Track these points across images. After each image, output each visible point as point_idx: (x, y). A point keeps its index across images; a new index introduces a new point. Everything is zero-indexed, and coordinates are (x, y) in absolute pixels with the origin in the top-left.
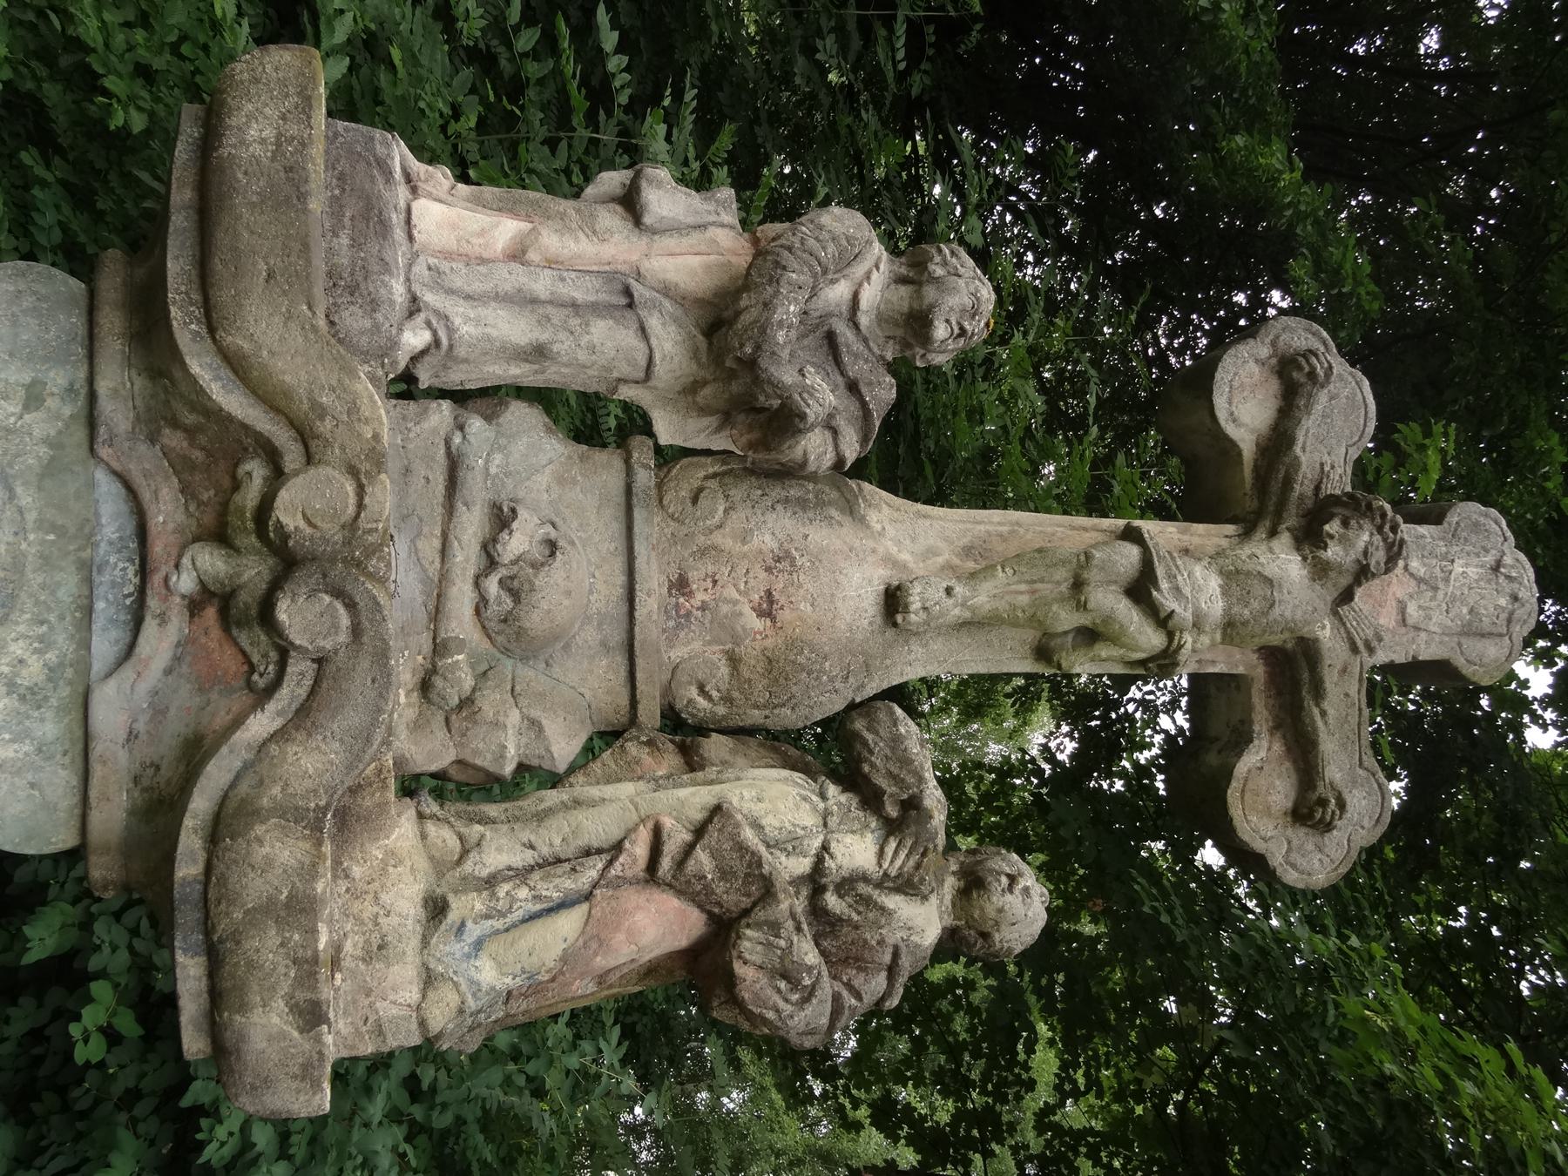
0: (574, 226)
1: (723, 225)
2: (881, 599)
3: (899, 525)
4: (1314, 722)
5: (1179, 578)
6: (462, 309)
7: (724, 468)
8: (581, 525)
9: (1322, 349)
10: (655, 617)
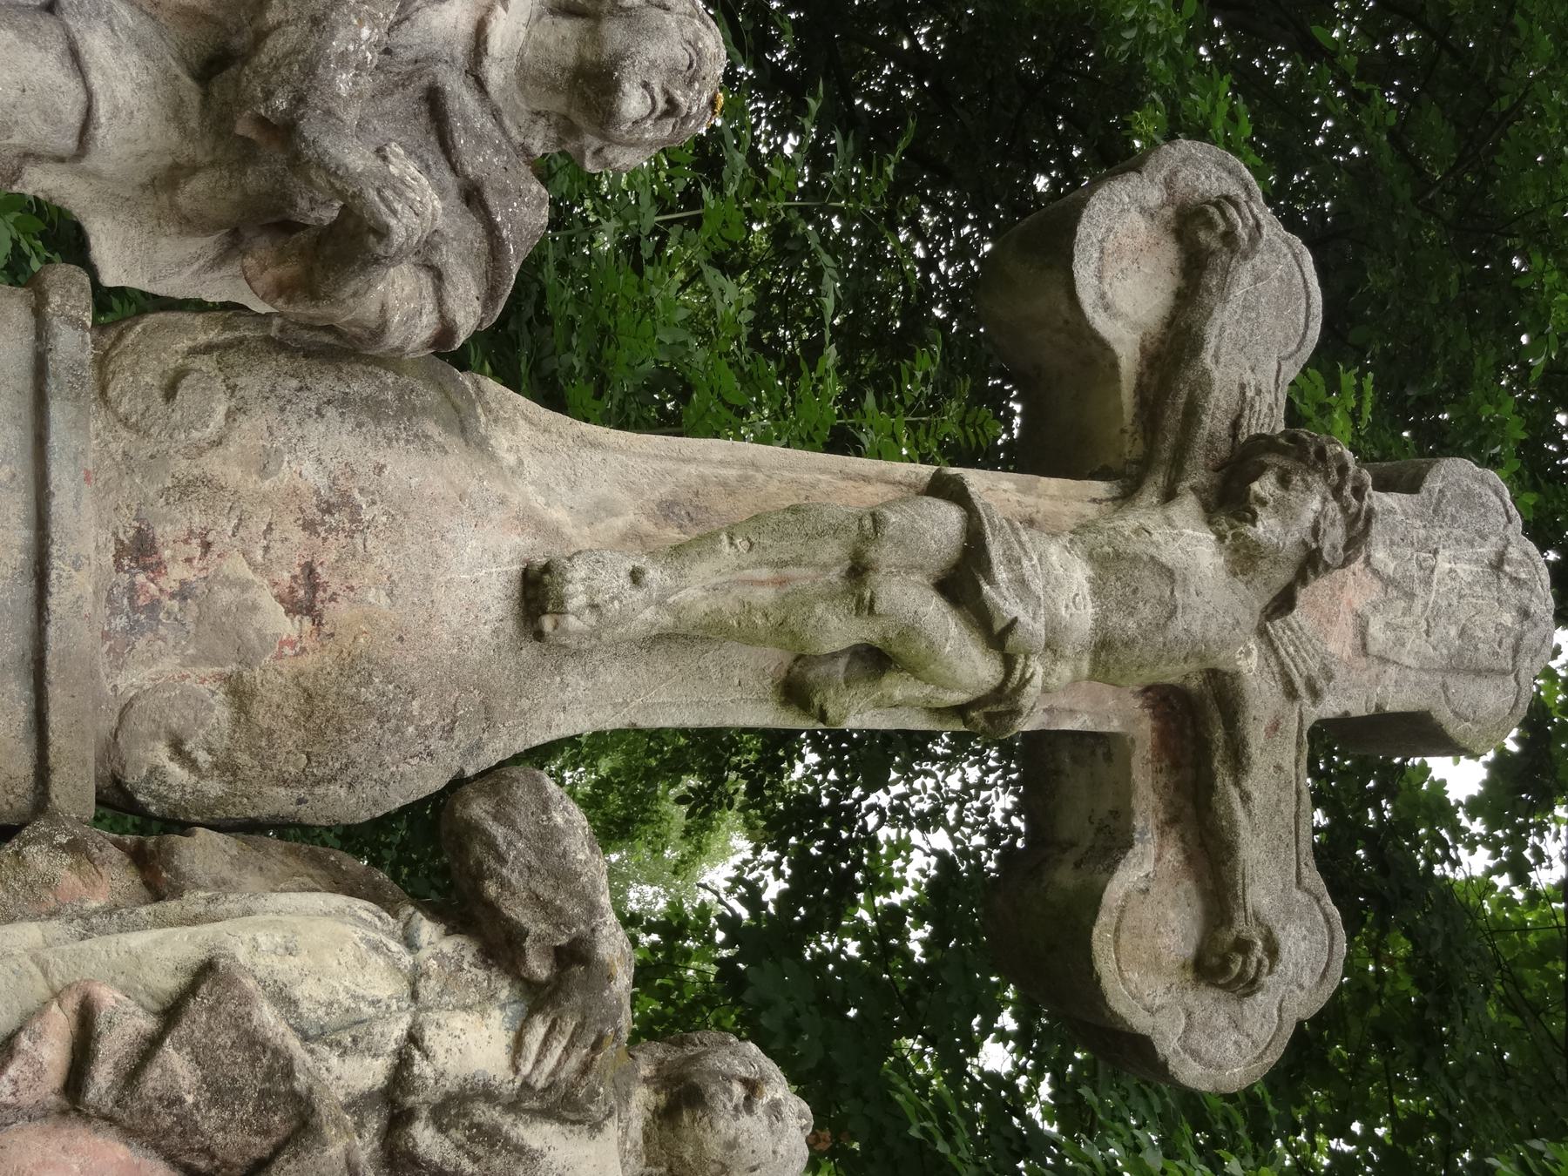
2: (515, 589)
3: (547, 458)
4: (1230, 811)
5: (1025, 563)
7: (228, 335)
9: (1243, 196)
10: (88, 608)
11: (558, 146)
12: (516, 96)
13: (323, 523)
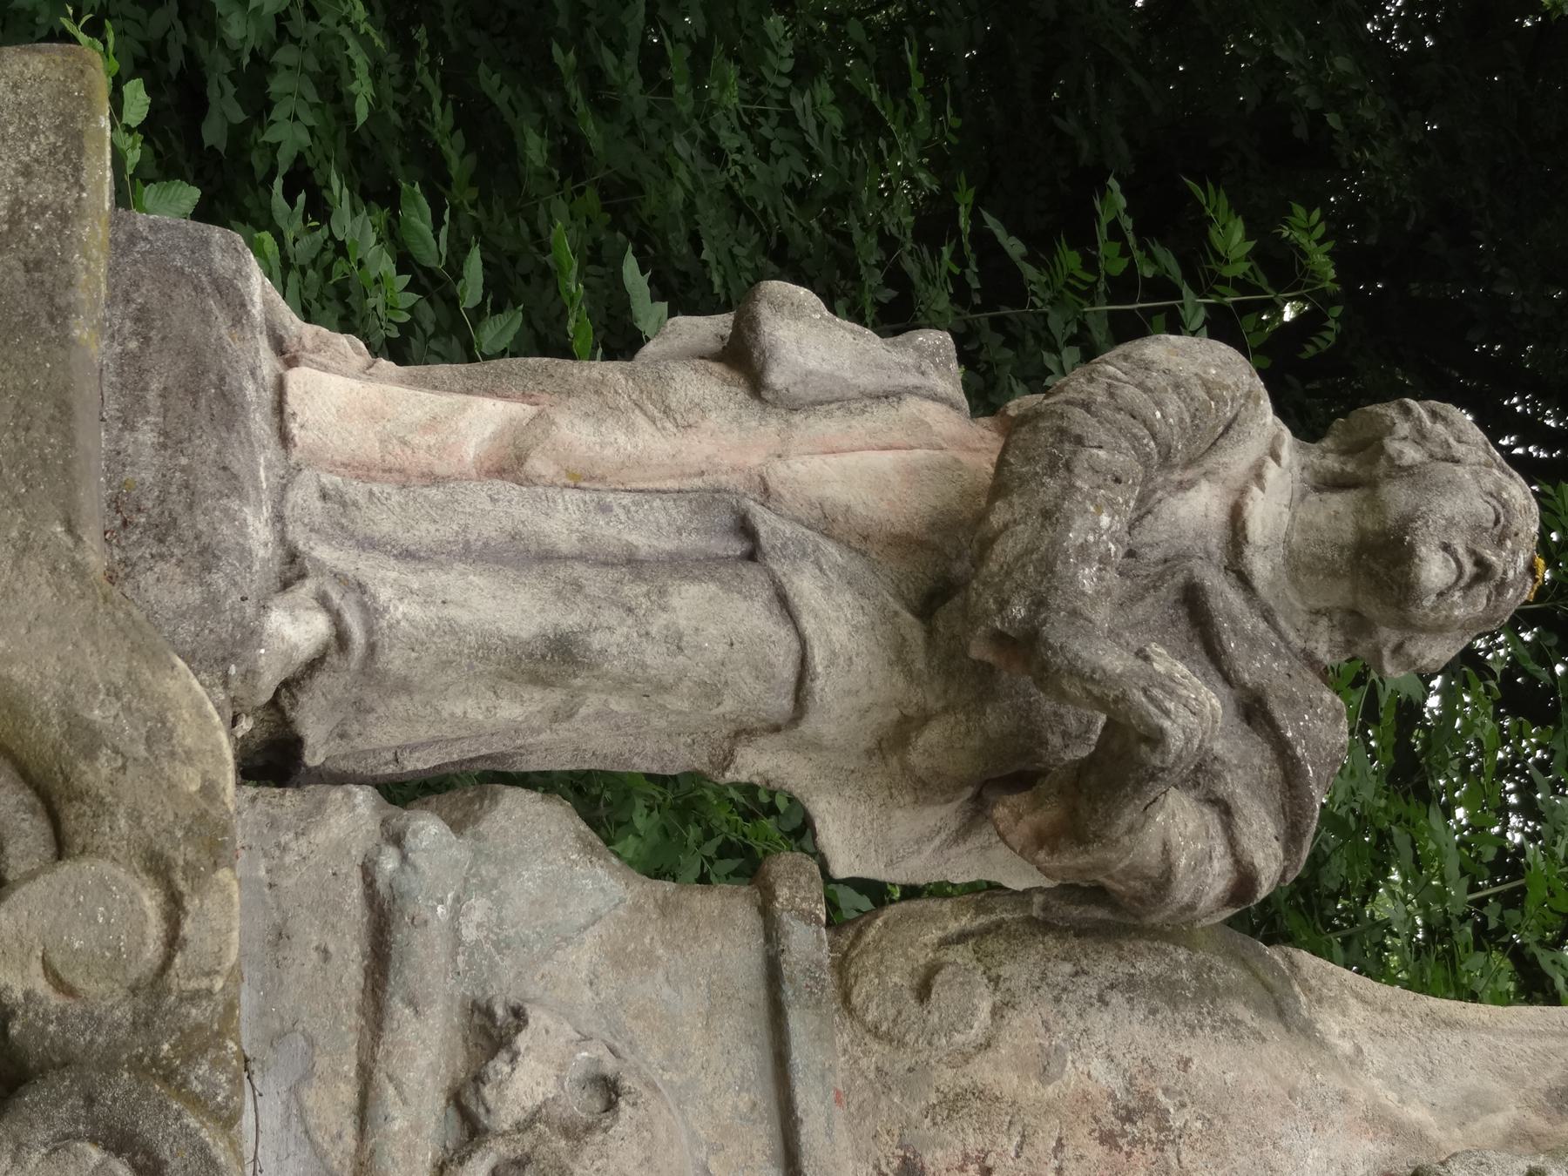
0: (623, 402)
1: (935, 397)
3: (1392, 1044)
6: (394, 575)
7: (983, 920)
8: (670, 1056)
11: (1347, 651)
12: (1289, 594)
13: (1124, 1134)
